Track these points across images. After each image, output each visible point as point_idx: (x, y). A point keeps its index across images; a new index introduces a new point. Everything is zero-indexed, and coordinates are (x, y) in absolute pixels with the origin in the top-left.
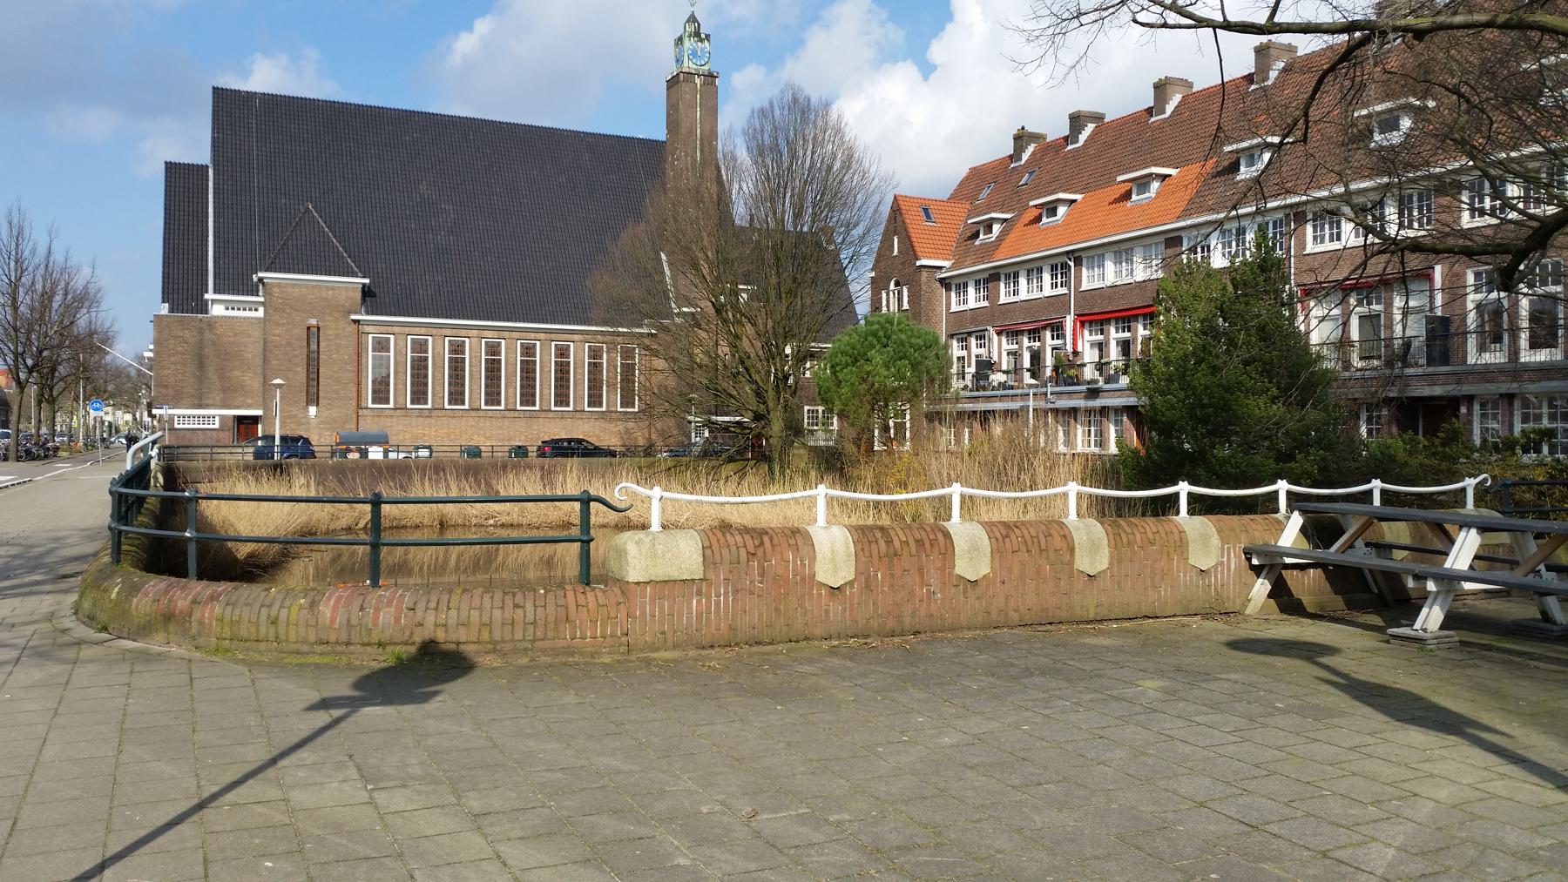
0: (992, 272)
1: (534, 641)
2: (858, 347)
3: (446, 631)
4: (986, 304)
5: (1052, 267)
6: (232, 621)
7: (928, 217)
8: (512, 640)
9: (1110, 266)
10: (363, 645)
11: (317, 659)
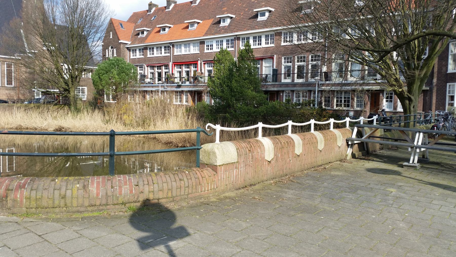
0: (145, 47)
1: (188, 195)
2: (108, 68)
3: (154, 194)
4: (143, 57)
5: (165, 47)
6: (36, 199)
7: (122, 27)
8: (180, 195)
9: (183, 48)
10: (114, 205)
11: (91, 214)
